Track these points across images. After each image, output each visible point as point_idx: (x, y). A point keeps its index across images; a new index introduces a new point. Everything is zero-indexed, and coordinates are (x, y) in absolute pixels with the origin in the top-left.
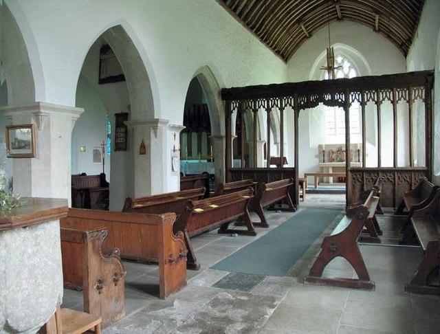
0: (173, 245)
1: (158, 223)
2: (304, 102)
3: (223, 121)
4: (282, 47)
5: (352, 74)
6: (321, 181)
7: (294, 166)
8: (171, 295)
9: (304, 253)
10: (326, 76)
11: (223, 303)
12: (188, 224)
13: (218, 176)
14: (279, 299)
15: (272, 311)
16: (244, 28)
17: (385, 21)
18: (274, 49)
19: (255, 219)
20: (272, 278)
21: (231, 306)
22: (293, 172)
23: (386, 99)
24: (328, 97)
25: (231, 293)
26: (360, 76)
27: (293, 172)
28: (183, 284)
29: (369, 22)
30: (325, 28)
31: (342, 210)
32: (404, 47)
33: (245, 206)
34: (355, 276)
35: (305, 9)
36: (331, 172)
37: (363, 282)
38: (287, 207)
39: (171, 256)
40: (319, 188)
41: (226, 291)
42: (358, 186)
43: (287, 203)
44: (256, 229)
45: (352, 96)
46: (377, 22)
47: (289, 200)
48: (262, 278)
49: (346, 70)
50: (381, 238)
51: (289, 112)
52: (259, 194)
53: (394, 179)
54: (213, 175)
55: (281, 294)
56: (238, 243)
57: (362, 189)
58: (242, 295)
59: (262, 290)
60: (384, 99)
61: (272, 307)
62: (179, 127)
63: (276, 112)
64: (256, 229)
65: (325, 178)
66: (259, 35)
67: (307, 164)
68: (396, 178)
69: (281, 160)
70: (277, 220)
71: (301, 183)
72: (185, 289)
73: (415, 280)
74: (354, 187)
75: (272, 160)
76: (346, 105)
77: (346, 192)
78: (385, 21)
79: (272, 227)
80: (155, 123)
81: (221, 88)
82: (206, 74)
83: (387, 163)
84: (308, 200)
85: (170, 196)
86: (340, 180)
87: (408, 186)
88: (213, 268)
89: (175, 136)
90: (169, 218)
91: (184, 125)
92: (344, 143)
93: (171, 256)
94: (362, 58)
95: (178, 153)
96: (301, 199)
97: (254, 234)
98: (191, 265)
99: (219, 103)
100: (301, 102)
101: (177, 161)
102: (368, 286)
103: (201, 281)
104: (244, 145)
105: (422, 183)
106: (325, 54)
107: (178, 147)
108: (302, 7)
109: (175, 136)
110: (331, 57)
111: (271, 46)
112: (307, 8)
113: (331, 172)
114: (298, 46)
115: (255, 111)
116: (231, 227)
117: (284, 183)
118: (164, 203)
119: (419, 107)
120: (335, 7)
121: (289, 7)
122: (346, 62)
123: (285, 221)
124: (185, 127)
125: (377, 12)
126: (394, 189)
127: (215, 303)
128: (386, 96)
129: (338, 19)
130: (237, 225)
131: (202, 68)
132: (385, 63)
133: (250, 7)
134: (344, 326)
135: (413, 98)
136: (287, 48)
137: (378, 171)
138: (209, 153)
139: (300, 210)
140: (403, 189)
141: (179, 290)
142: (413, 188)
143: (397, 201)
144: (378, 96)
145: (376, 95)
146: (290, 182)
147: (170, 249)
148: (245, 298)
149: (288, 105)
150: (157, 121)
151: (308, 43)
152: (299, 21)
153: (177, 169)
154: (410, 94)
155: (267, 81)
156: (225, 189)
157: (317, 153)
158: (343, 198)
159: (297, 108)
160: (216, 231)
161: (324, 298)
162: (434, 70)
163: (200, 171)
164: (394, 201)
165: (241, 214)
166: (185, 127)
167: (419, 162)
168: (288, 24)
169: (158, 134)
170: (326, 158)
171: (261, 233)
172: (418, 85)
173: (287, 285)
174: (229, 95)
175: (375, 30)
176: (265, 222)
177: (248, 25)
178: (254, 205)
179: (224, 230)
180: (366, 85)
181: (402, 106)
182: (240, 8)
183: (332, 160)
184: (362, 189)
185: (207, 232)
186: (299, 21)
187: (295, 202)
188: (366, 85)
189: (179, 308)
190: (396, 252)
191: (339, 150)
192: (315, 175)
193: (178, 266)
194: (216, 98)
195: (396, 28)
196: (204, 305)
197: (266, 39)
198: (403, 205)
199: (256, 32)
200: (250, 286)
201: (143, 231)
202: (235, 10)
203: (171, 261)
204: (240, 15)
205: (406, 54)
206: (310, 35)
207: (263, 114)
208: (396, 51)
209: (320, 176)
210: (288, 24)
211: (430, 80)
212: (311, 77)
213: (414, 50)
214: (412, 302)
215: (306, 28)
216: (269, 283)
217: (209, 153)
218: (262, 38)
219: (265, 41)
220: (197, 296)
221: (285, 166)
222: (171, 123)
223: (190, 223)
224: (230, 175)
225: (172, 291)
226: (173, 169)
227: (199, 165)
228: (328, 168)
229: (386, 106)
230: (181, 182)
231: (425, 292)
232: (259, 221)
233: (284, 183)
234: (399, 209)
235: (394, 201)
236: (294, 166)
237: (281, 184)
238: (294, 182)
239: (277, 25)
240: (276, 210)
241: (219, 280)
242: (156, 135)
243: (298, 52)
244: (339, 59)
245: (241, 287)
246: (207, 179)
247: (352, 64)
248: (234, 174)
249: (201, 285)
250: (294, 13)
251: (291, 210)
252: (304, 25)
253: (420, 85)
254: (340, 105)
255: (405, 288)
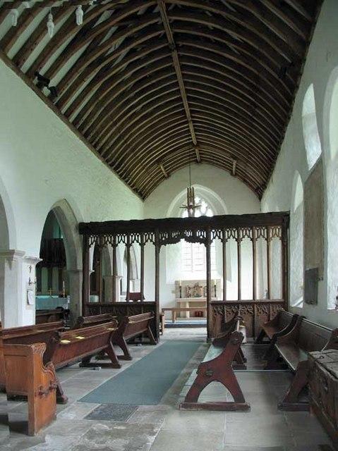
0: (42, 376)
1: (27, 356)
2: (203, 237)
3: (78, 256)
4: (140, 186)
5: (210, 214)
6: (178, 316)
7: (154, 300)
8: (41, 431)
9: (173, 382)
10: (185, 215)
11: (100, 435)
12: (54, 357)
13: (73, 310)
14: (158, 426)
15: (153, 438)
16: (104, 165)
17: (242, 166)
18: (132, 187)
19: (119, 352)
20: (146, 407)
21: (110, 437)
22: (153, 306)
23: (246, 236)
24: (189, 234)
25: (106, 424)
26: (217, 215)
27: (153, 306)
28: (53, 418)
29: (226, 166)
30: (186, 170)
31: (203, 341)
32: (259, 191)
33: (109, 338)
34: (230, 399)
35: (164, 151)
36: (188, 307)
37: (238, 405)
38: (148, 340)
39: (41, 388)
40: (177, 322)
41: (100, 422)
42: (219, 317)
43: (148, 337)
44: (121, 362)
45: (213, 233)
46: (234, 167)
47: (150, 333)
48: (135, 407)
49: (205, 210)
50: (245, 364)
51: (150, 247)
52: (123, 326)
53: (254, 311)
54: (68, 311)
55: (158, 421)
56: (104, 376)
57: (223, 321)
58: (119, 425)
59: (142, 417)
60: (244, 237)
61: (154, 434)
62: (35, 260)
63: (136, 247)
64: (121, 362)
65: (182, 313)
66: (118, 173)
67: (167, 299)
68: (256, 311)
69: (140, 295)
70: (140, 353)
71: (161, 317)
72: (55, 424)
73: (287, 399)
74: (214, 319)
75: (130, 295)
76: (207, 242)
77: (207, 326)
78: (242, 166)
79: (136, 359)
80: (10, 255)
81: (79, 221)
82: (64, 207)
83: (247, 296)
84: (167, 334)
85: (28, 329)
86: (198, 314)
87: (266, 318)
88: (81, 400)
89: (30, 268)
90: (39, 349)
91: (40, 257)
92: (206, 279)
93: (41, 388)
94: (219, 199)
95: (34, 286)
96: (160, 333)
97: (119, 367)
98: (60, 400)
99: (76, 237)
100: (162, 238)
101: (33, 293)
102: (245, 408)
103: (71, 414)
104: (100, 281)
105: (280, 313)
106: (185, 192)
107: (34, 279)
108: (163, 148)
109: (30, 268)
110: (191, 196)
111: (129, 184)
112: (167, 150)
113: (188, 307)
114: (155, 185)
115: (115, 246)
116: (93, 361)
117: (144, 316)
118: (22, 336)
119: (277, 245)
120: (194, 150)
121: (150, 147)
122: (203, 203)
123: (147, 353)
124: (42, 260)
125: (235, 158)
126: (254, 320)
127: (92, 435)
128: (231, 234)
129: (196, 161)
130: (99, 359)
131: (59, 201)
132: (242, 205)
133: (110, 144)
134: (227, 446)
135: (271, 236)
136: (144, 187)
137: (238, 304)
138: (60, 288)
139: (160, 343)
140: (261, 320)
141: (49, 424)
142: (271, 319)
143: (256, 332)
144: (267, 232)
145: (236, 232)
146: (151, 315)
147: (40, 381)
148: (123, 428)
149: (246, 236)
150: (12, 252)
151: (165, 183)
152: (158, 162)
153: (33, 302)
154: (115, 238)
155: (127, 217)
156: (85, 322)
157: (174, 289)
158: (204, 331)
159: (158, 244)
160: (78, 365)
161: (203, 421)
162: (289, 212)
163: (53, 307)
164: (253, 329)
165: (106, 346)
166: (42, 260)
167: (277, 295)
168: (148, 163)
169: (13, 267)
170: (183, 294)
171: (125, 366)
172: (276, 224)
173: (164, 412)
174: (87, 229)
175: (232, 174)
176: (128, 354)
177: (107, 161)
178: (117, 339)
179: (86, 363)
180: (223, 224)
181: (261, 243)
182: (101, 144)
183: (188, 296)
184: (223, 321)
185: (67, 366)
186: (158, 162)
187: (156, 336)
188: (223, 224)
189: (52, 444)
190: (262, 377)
191: (197, 286)
192: (172, 310)
193: (48, 399)
194: (73, 232)
195: (252, 173)
196: (79, 439)
197: (125, 176)
198: (263, 334)
199: (115, 169)
200: (126, 416)
201: (8, 364)
202: (95, 146)
203: (41, 394)
204: (100, 151)
205: (260, 198)
206: (169, 175)
207: (121, 248)
208: (254, 196)
209: (177, 311)
210: (148, 163)
211: (286, 221)
212: (169, 214)
213: (269, 194)
214: (287, 419)
215: (165, 168)
216: (144, 412)
217: (60, 288)
218: (121, 176)
219: (124, 178)
220: (70, 429)
221: (144, 301)
222: (28, 255)
223: (56, 355)
224: (87, 309)
225: (41, 427)
226: (28, 303)
227: (53, 301)
228: (185, 303)
229: (246, 244)
230: (36, 317)
231: (297, 409)
232: (123, 354)
233: (144, 316)
234: (259, 338)
235: (253, 329)
236: (154, 300)
237: (141, 318)
238: (155, 315)
239: (137, 164)
240: (137, 344)
241: (89, 412)
242: (10, 267)
243: (156, 190)
244: (197, 200)
245: (115, 417)
246: (62, 314)
247: (209, 204)
248: (92, 309)
249: (72, 418)
250: (155, 153)
251: (153, 343)
252: (164, 165)
253: (278, 225)
254: (201, 241)
255: (279, 407)
